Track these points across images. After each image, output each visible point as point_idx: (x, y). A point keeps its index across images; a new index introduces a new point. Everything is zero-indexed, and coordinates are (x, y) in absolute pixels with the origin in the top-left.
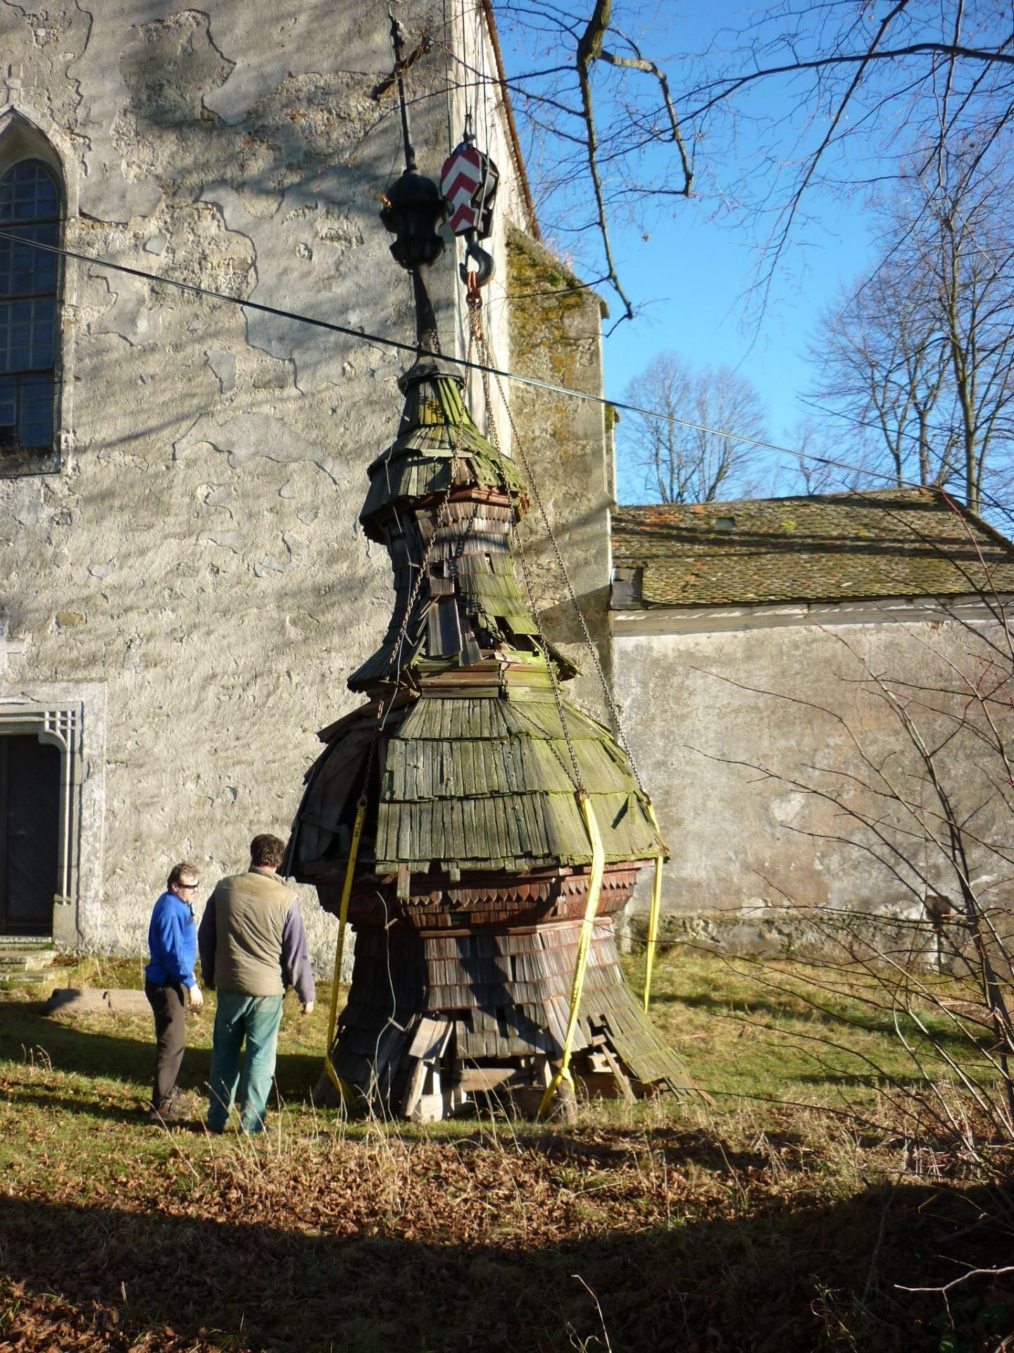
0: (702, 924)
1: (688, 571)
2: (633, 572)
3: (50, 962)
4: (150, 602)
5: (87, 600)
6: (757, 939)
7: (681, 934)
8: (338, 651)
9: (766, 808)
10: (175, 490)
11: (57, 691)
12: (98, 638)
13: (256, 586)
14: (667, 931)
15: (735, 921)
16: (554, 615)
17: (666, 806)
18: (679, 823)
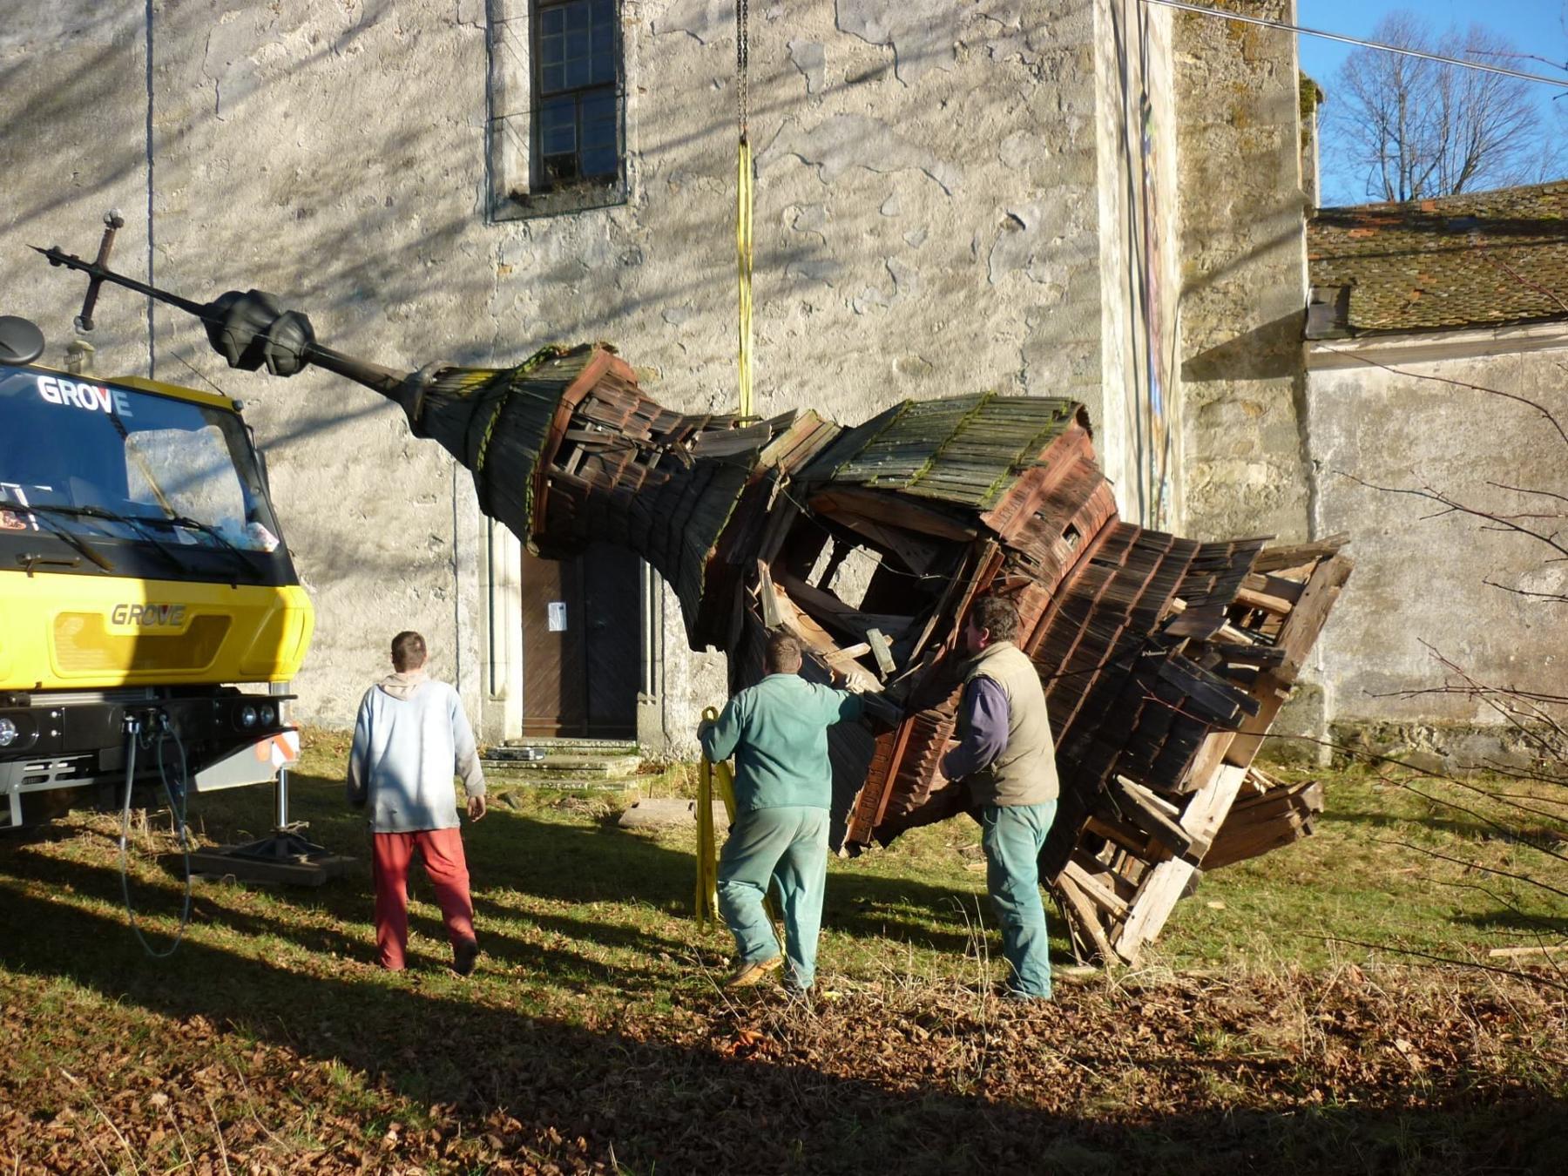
0: (1425, 732)
1: (1410, 286)
2: (1338, 291)
3: (635, 768)
5: (662, 352)
6: (1497, 752)
7: (1396, 745)
12: (676, 395)
13: (856, 325)
14: (1379, 740)
15: (1469, 729)
17: (1377, 585)
18: (1394, 606)
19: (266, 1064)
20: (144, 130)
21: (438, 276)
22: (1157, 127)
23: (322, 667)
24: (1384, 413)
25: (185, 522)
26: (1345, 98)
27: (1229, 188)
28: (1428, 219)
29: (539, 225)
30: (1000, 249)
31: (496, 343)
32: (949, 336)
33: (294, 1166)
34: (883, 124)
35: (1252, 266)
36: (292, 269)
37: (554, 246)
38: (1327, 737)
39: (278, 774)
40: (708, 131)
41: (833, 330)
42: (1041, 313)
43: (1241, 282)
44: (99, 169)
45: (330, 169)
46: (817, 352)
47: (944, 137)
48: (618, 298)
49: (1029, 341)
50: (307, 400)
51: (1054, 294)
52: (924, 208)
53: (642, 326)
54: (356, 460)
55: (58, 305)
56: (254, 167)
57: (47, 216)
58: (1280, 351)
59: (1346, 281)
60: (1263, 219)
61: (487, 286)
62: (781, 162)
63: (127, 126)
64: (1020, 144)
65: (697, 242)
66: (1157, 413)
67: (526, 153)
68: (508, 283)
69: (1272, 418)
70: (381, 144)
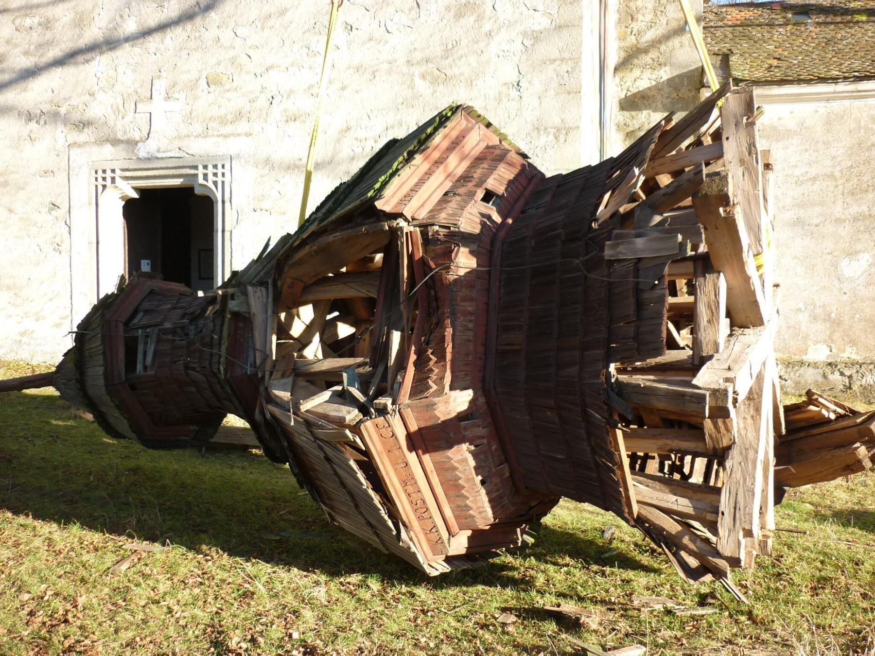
2: (720, 58)
9: (835, 266)
15: (802, 363)
16: (650, 93)
59: (725, 50)
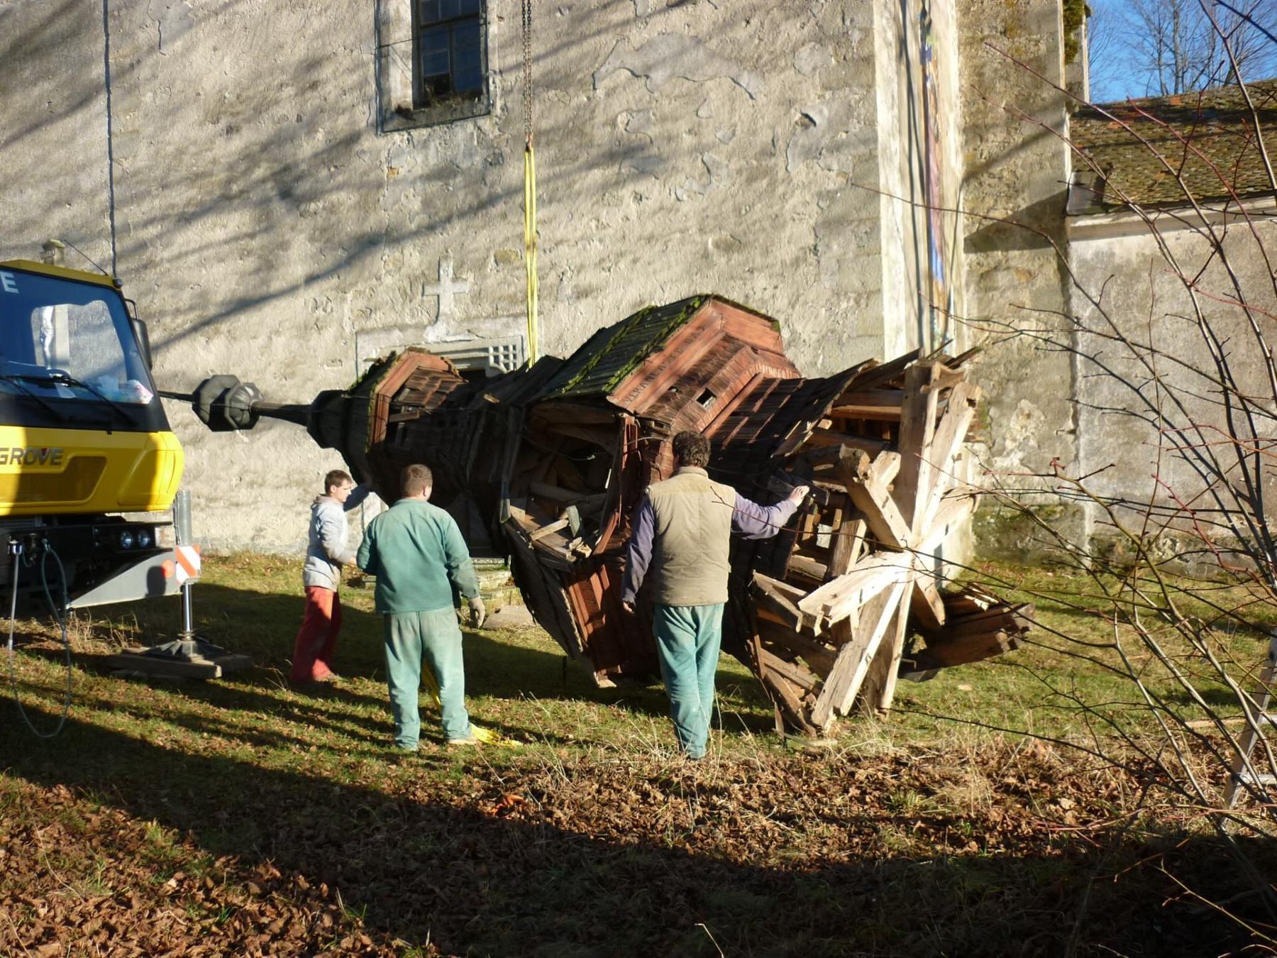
0: (1169, 542)
4: (578, 234)
8: (760, 271)
10: (596, 120)
11: (499, 327)
13: (678, 210)
16: (1007, 226)
19: (102, 824)
20: (103, 65)
21: (340, 179)
22: (938, 38)
23: (255, 502)
24: (1134, 276)
25: (65, 378)
26: (1128, 16)
27: (1003, 89)
28: (1176, 111)
29: (420, 134)
30: (796, 144)
31: (387, 233)
32: (755, 217)
33: (79, 909)
34: (698, 41)
35: (1022, 155)
36: (223, 176)
37: (432, 151)
38: (1087, 548)
39: (183, 588)
40: (555, 51)
41: (659, 215)
42: (830, 196)
43: (1013, 168)
44: (67, 98)
45: (251, 93)
46: (646, 234)
47: (748, 51)
48: (485, 193)
49: (820, 220)
50: (237, 284)
51: (841, 180)
52: (732, 110)
53: (504, 216)
54: (277, 333)
55: (39, 211)
56: (191, 93)
57: (28, 138)
58: (1045, 225)
60: (1031, 115)
61: (379, 185)
62: (614, 76)
63: (87, 62)
64: (811, 54)
65: (548, 144)
66: (938, 280)
67: (409, 75)
68: (396, 182)
69: (1040, 282)
70: (292, 70)
